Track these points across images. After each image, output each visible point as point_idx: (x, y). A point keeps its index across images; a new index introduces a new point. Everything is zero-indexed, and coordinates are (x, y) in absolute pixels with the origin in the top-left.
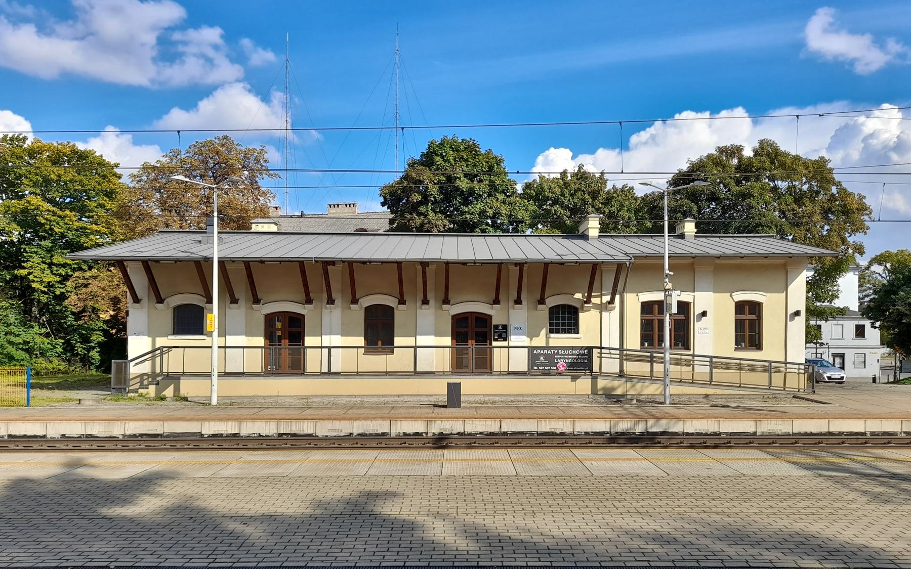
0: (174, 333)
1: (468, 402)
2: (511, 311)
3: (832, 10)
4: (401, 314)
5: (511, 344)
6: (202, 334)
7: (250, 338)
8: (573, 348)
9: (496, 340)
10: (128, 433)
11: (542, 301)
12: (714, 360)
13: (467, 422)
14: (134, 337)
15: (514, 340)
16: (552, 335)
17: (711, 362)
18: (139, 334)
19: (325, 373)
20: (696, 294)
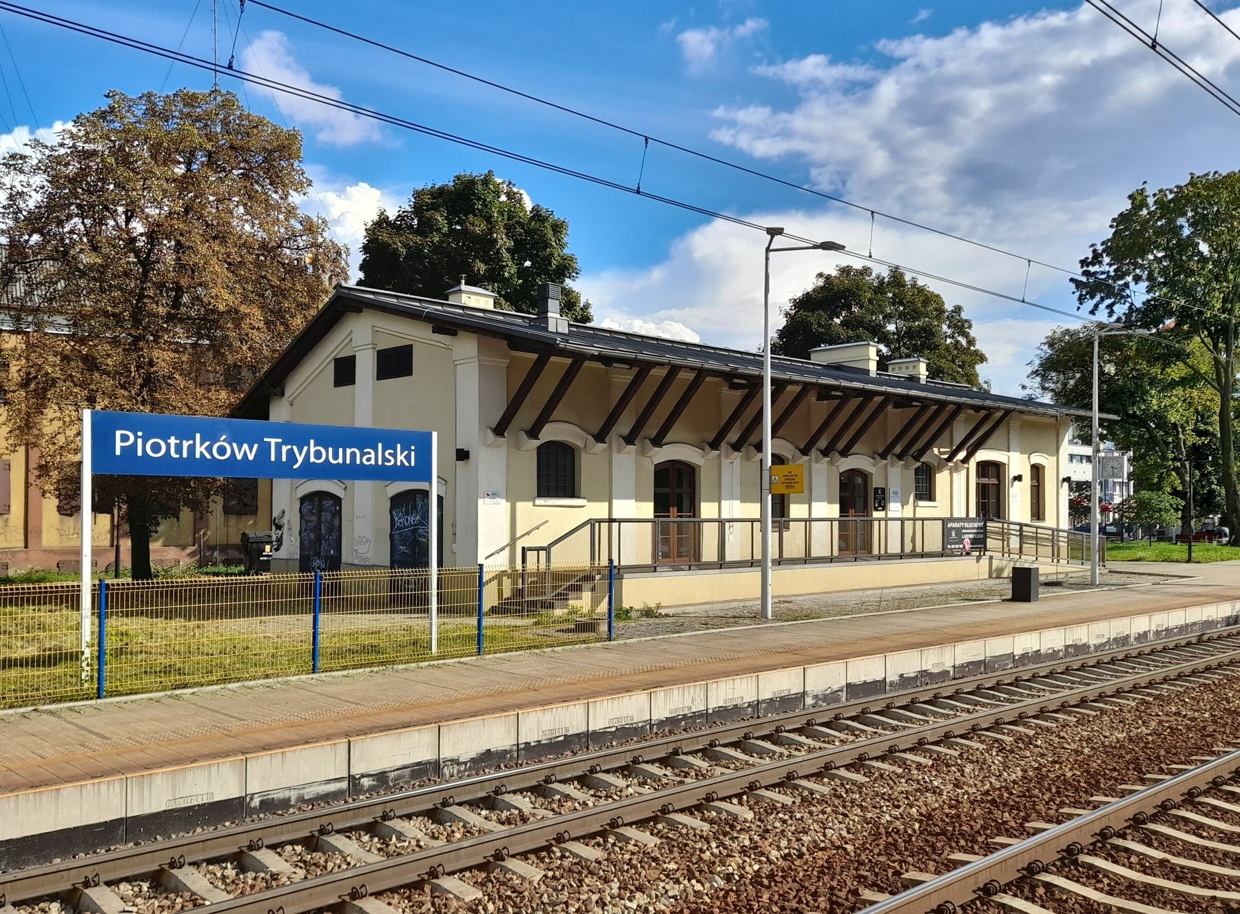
0: (540, 495)
1: (360, 587)
2: (615, 455)
3: (767, 25)
4: (591, 460)
5: (890, 515)
6: (573, 495)
7: (640, 504)
8: (27, 485)
9: (876, 509)
10: (958, 663)
11: (533, 433)
12: (1025, 528)
13: (1188, 610)
14: (487, 500)
15: (895, 509)
16: (921, 503)
17: (1021, 530)
18: (495, 495)
19: (794, 561)
20: (1011, 454)
